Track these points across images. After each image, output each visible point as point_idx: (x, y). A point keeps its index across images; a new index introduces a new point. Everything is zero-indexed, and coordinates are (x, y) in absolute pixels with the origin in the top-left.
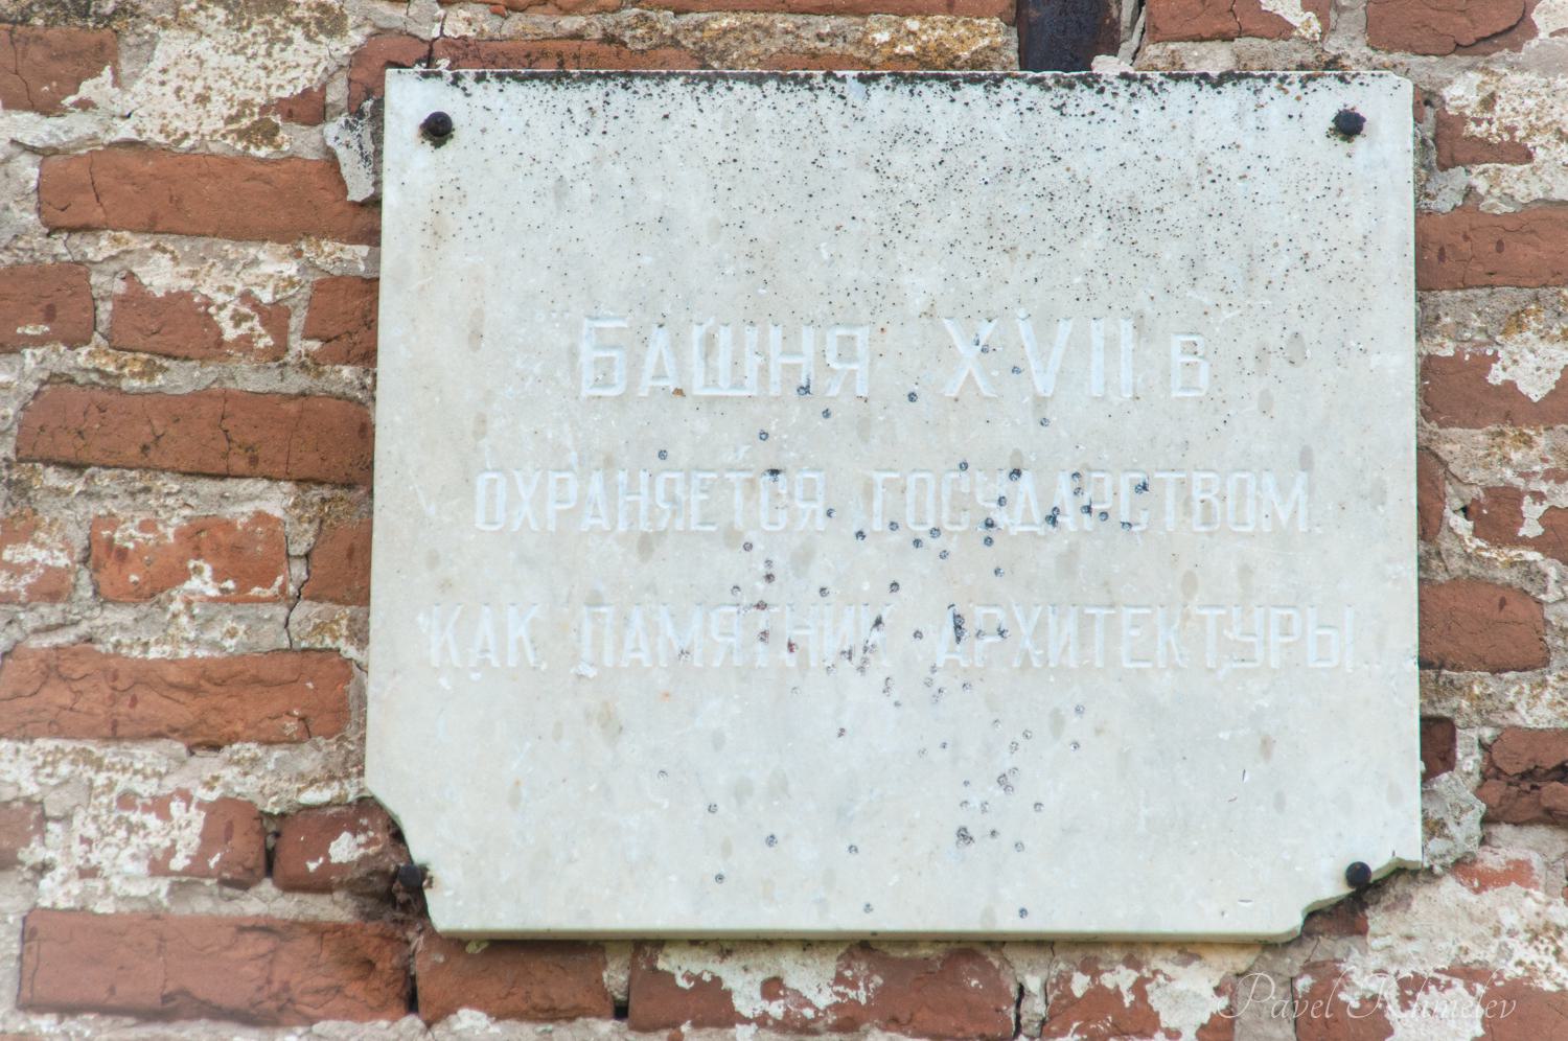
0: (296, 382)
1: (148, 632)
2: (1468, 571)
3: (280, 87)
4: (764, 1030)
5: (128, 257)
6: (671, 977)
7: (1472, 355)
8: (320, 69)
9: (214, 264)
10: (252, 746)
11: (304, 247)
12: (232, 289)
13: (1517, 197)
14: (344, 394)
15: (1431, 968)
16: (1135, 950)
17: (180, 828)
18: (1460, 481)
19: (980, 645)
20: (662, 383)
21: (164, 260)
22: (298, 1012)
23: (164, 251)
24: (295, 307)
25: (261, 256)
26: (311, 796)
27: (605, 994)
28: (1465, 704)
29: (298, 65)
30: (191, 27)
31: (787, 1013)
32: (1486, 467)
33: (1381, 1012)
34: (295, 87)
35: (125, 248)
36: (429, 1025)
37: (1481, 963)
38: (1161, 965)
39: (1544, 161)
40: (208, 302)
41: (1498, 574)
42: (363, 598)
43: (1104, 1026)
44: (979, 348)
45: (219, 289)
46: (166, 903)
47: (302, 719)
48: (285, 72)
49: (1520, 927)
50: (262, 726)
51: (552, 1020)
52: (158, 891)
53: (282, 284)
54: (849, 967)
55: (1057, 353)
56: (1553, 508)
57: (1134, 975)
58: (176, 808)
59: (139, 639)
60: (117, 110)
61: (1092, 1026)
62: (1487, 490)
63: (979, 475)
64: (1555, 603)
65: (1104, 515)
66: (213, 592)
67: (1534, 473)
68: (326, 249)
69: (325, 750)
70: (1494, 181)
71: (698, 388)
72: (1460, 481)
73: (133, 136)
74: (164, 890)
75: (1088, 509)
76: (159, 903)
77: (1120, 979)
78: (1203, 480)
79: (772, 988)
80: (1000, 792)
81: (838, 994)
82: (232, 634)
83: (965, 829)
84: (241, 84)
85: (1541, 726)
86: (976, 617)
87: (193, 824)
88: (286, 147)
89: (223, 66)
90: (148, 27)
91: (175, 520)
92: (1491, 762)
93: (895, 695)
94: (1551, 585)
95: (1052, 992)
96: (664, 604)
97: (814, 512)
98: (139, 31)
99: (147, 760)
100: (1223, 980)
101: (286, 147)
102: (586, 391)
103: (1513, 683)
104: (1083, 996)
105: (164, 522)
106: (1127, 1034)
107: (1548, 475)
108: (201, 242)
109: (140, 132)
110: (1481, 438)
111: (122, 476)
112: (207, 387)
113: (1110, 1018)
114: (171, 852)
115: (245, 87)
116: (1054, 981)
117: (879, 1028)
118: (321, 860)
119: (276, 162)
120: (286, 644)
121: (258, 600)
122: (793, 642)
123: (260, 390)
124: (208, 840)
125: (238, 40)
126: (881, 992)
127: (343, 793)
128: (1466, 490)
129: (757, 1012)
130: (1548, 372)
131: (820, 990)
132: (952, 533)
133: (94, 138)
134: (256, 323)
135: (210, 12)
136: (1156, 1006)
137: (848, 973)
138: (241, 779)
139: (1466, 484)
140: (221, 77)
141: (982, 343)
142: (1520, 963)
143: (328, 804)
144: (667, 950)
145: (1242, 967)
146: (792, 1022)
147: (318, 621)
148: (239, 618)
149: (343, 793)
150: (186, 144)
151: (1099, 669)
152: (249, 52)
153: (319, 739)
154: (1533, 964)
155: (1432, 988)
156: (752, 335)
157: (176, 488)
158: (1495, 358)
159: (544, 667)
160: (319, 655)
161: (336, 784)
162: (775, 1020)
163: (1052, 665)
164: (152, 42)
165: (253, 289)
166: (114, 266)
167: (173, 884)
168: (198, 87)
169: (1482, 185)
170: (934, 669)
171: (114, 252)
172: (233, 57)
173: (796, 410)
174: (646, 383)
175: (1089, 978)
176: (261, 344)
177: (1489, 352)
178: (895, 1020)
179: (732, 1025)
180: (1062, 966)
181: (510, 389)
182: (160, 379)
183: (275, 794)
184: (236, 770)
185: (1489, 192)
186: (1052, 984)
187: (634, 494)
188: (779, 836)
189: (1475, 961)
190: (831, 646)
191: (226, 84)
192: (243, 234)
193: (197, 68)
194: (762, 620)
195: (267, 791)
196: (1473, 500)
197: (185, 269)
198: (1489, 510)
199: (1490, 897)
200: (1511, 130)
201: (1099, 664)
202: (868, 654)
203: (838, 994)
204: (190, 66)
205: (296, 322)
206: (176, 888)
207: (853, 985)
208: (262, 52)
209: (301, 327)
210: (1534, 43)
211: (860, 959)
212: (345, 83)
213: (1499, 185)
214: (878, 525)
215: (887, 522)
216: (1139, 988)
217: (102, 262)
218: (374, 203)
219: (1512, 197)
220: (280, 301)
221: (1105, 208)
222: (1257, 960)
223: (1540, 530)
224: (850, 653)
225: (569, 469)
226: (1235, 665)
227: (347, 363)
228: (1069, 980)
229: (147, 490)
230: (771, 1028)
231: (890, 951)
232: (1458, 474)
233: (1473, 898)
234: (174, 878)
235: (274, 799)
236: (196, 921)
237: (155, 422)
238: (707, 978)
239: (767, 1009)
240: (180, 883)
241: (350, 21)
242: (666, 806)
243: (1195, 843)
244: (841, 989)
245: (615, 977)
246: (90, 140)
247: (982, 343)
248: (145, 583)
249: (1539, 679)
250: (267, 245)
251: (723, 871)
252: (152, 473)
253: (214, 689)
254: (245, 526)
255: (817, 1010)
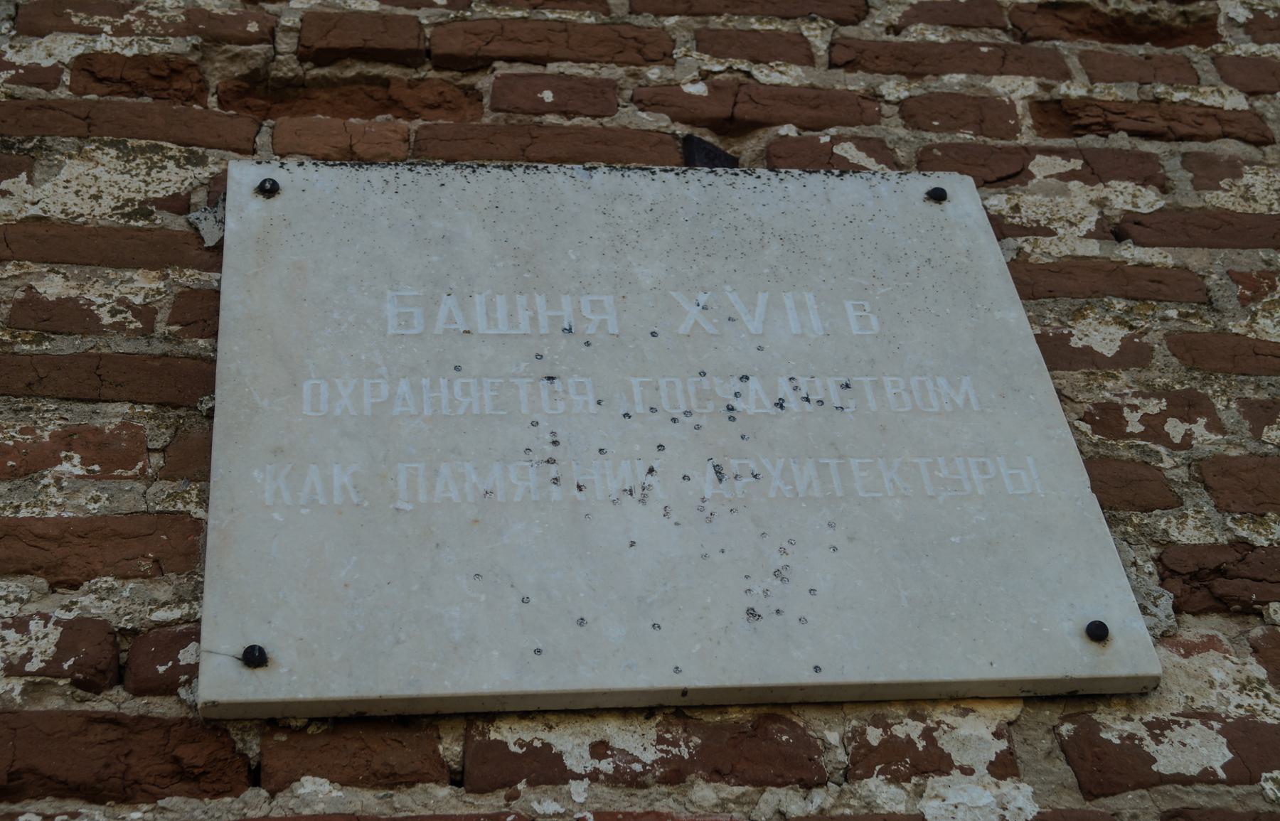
0: (158, 348)
1: (20, 498)
2: (1098, 453)
3: (156, 192)
4: (597, 784)
5: (28, 277)
6: (504, 744)
7: (1054, 334)
8: (186, 183)
9: (97, 281)
10: (110, 579)
11: (170, 272)
12: (111, 296)
13: (1053, 253)
14: (200, 354)
15: (1168, 714)
16: (916, 707)
17: (37, 639)
18: (1072, 400)
19: (738, 484)
20: (454, 326)
21: (58, 279)
22: (144, 791)
23: (58, 273)
24: (161, 308)
25: (135, 277)
26: (161, 615)
27: (442, 763)
28: (1130, 529)
29: (170, 181)
30: (91, 160)
31: (617, 768)
32: (1090, 391)
33: (1140, 746)
34: (167, 192)
35: (26, 270)
36: (273, 795)
37: (1207, 708)
38: (942, 718)
39: (1065, 235)
40: (91, 303)
41: (1121, 453)
42: (206, 477)
43: (905, 767)
44: (700, 307)
45: (100, 296)
46: (19, 700)
47: (156, 561)
48: (160, 184)
49: (1229, 681)
50: (120, 564)
51: (391, 787)
52: (12, 690)
53: (151, 293)
54: (668, 731)
55: (760, 310)
56: (1146, 415)
57: (921, 726)
58: (35, 626)
59: (11, 503)
60: (29, 198)
61: (893, 767)
62: (1094, 405)
63: (715, 379)
64: (1171, 468)
65: (821, 402)
66: (79, 471)
67: (1126, 394)
68: (188, 273)
69: (176, 582)
70: (1035, 245)
71: (481, 326)
72: (1072, 400)
73: (41, 213)
74: (18, 689)
75: (807, 400)
76: (13, 700)
77: (909, 729)
78: (891, 381)
79: (600, 749)
80: (777, 582)
81: (662, 751)
82: (96, 500)
83: (753, 609)
84: (126, 190)
85: (1193, 542)
86: (732, 466)
87: (50, 636)
88: (158, 222)
89: (112, 180)
90: (58, 156)
91: (51, 427)
92: (1166, 567)
93: (674, 518)
94: (1165, 457)
95: (850, 745)
96: (468, 461)
97: (586, 403)
98: (51, 158)
99: (11, 589)
100: (998, 727)
101: (158, 222)
102: (391, 331)
103: (1162, 517)
104: (879, 744)
105: (42, 429)
106: (927, 773)
107: (1135, 395)
108: (87, 269)
109: (45, 212)
110: (1079, 376)
111: (9, 400)
112: (86, 351)
113: (908, 760)
114: (28, 657)
115: (129, 191)
116: (850, 735)
117: (704, 779)
118: (170, 664)
119: (150, 230)
120: (143, 507)
121: (120, 477)
122: (581, 484)
123: (131, 351)
124: (63, 648)
125: (125, 167)
126: (701, 749)
127: (192, 611)
128: (1078, 406)
129: (588, 770)
130: (1111, 341)
131: (645, 749)
132: (702, 414)
133: (10, 213)
134: (129, 315)
135: (105, 151)
136: (947, 749)
137: (668, 736)
138: (97, 604)
139: (1076, 403)
140: (111, 186)
141: (701, 305)
142: (1239, 706)
143: (176, 622)
144: (498, 723)
145: (1012, 717)
146: (622, 775)
147: (171, 491)
148: (103, 490)
149: (192, 611)
150: (81, 220)
151: (841, 498)
152: (134, 173)
153: (170, 575)
154: (1249, 705)
155: (1175, 727)
156: (521, 300)
157: (54, 407)
158: (1071, 334)
159: (366, 504)
160: (173, 517)
161: (186, 605)
162: (606, 775)
163: (800, 495)
164: (60, 166)
165: (128, 296)
166: (16, 282)
167: (27, 684)
168: (93, 191)
169: (1028, 249)
170: (703, 500)
171: (17, 273)
172: (121, 176)
173: (563, 342)
174: (440, 326)
175: (881, 730)
176: (132, 326)
177: (1066, 332)
178: (718, 772)
179: (566, 783)
180: (854, 723)
181: (329, 330)
182: (46, 345)
183: (129, 614)
184: (93, 596)
185: (1032, 251)
186: (848, 738)
187: (433, 397)
188: (588, 618)
189: (1202, 707)
190: (614, 486)
191: (115, 191)
192: (120, 264)
193: (93, 181)
194: (553, 471)
195: (121, 612)
196: (1085, 412)
197: (73, 283)
198: (1100, 417)
199: (1196, 660)
200: (1038, 222)
201: (839, 494)
202: (646, 491)
203: (662, 751)
204: (88, 181)
205: (162, 316)
206: (30, 689)
207: (675, 744)
208: (144, 172)
209: (166, 319)
210: (1035, 181)
211: (677, 725)
212: (205, 194)
213: (1039, 247)
214: (639, 409)
215: (647, 408)
216: (927, 734)
217: (6, 279)
218: (219, 248)
219: (1049, 253)
220: (149, 303)
221: (777, 234)
222: (1021, 712)
223: (1142, 428)
224: (631, 491)
225: (381, 377)
226: (949, 494)
227: (201, 338)
228: (864, 733)
229: (29, 409)
230: (603, 782)
231: (703, 717)
232: (1070, 395)
233: (1185, 661)
234: (29, 679)
235: (128, 617)
236: (50, 715)
237: (39, 370)
238: (537, 744)
239: (598, 766)
240: (34, 684)
241: (210, 159)
242: (483, 598)
243: (953, 614)
244: (664, 747)
245: (451, 748)
246: (6, 215)
247: (701, 305)
248: (20, 467)
249: (1180, 513)
250: (140, 271)
251: (540, 646)
252: (34, 398)
253: (76, 540)
254: (112, 431)
255: (645, 765)
